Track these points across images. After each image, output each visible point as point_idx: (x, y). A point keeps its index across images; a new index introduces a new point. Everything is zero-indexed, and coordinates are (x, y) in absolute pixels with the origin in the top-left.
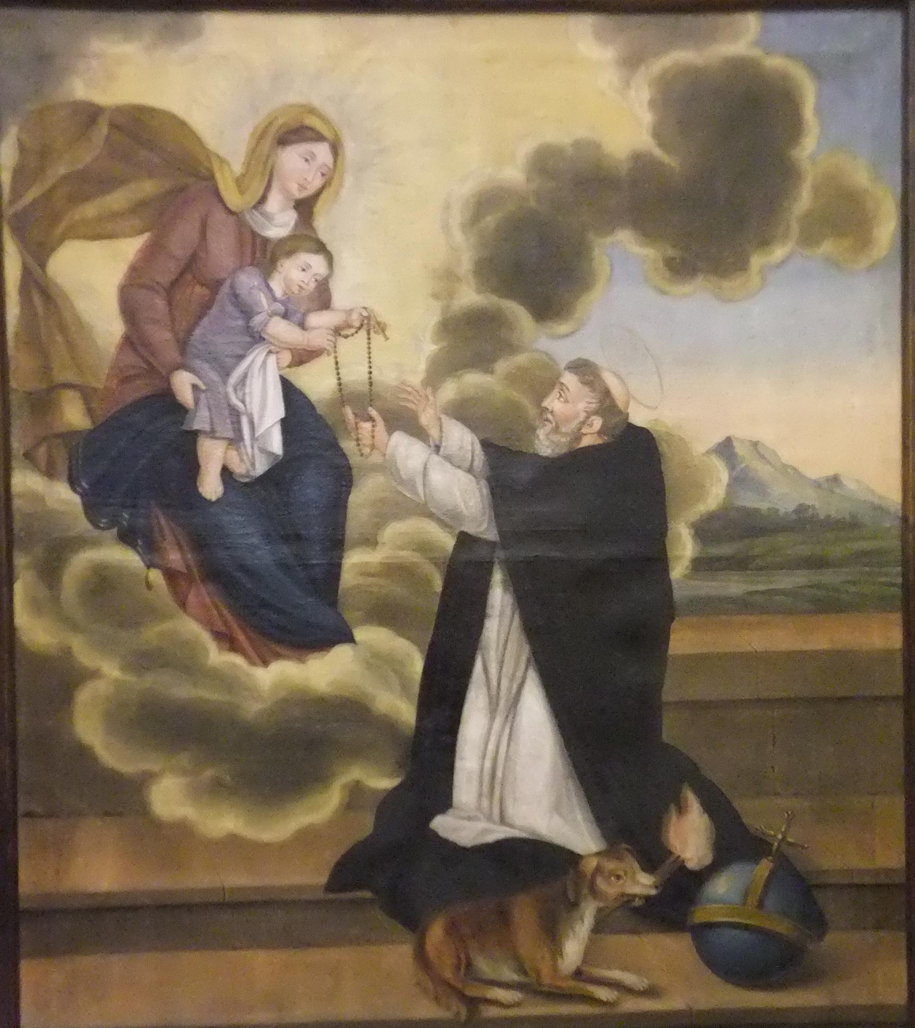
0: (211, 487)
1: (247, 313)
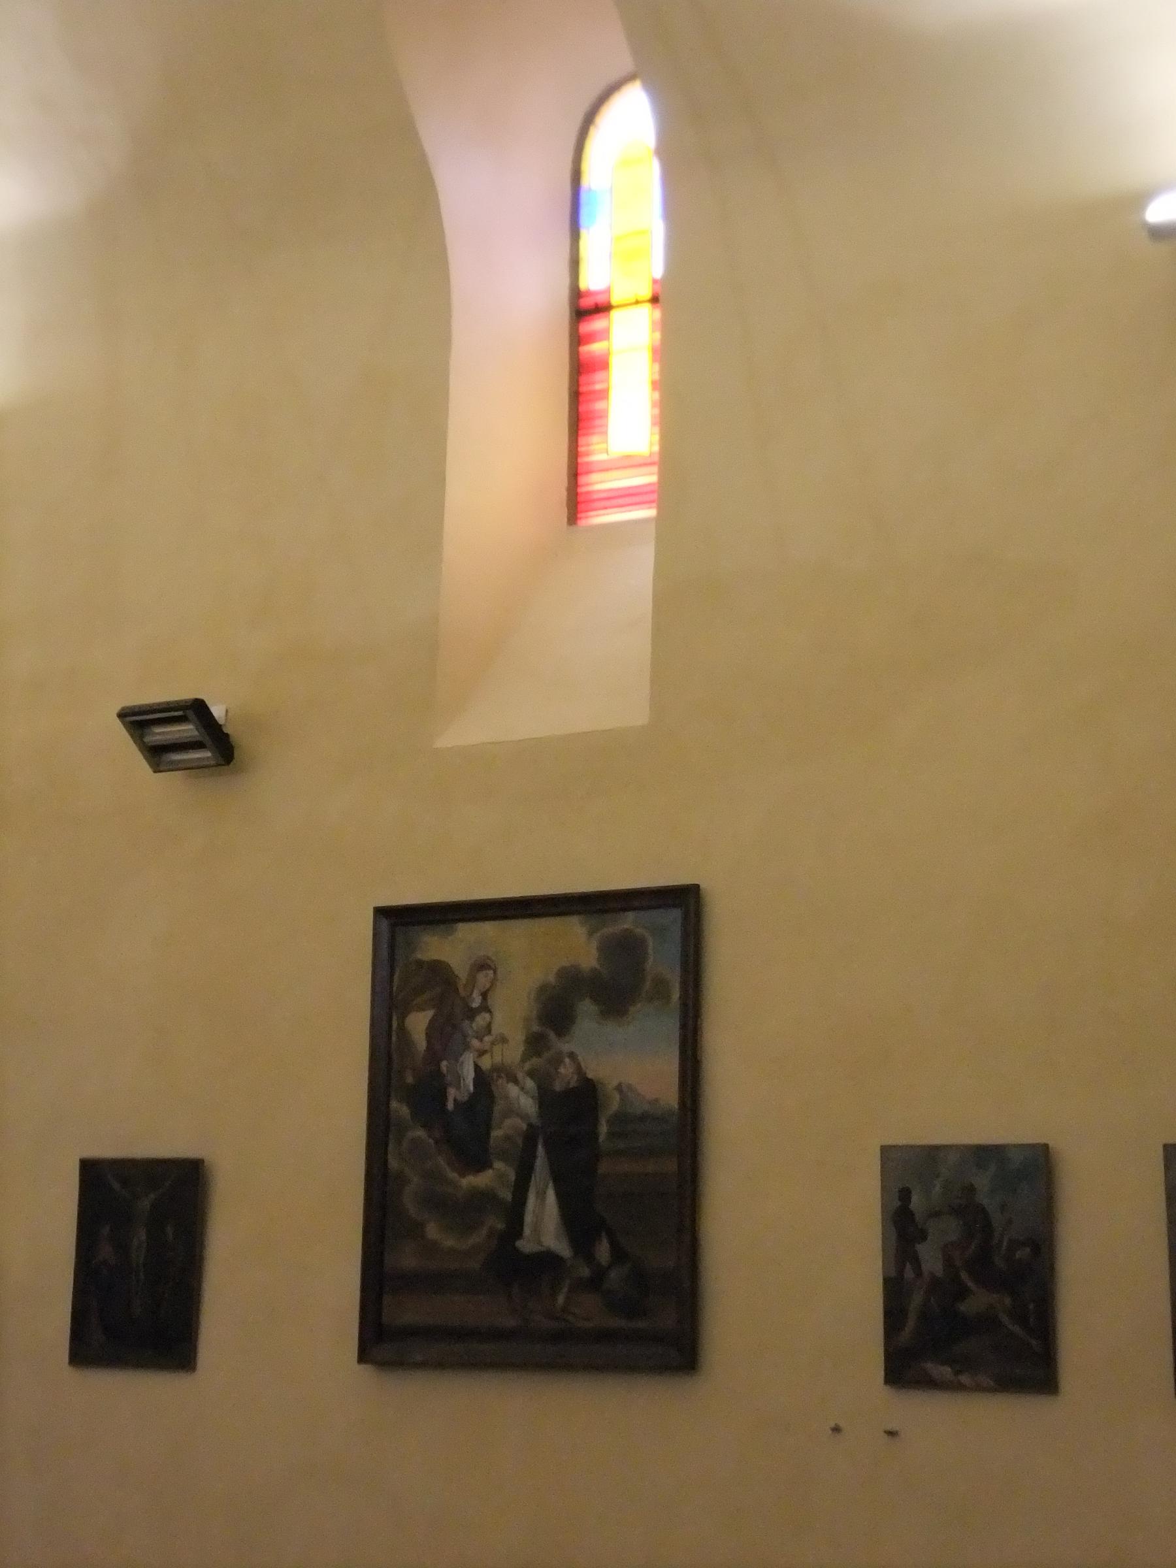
0: (450, 1106)
1: (465, 1036)
